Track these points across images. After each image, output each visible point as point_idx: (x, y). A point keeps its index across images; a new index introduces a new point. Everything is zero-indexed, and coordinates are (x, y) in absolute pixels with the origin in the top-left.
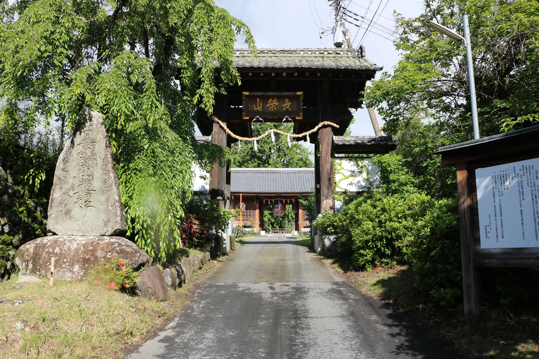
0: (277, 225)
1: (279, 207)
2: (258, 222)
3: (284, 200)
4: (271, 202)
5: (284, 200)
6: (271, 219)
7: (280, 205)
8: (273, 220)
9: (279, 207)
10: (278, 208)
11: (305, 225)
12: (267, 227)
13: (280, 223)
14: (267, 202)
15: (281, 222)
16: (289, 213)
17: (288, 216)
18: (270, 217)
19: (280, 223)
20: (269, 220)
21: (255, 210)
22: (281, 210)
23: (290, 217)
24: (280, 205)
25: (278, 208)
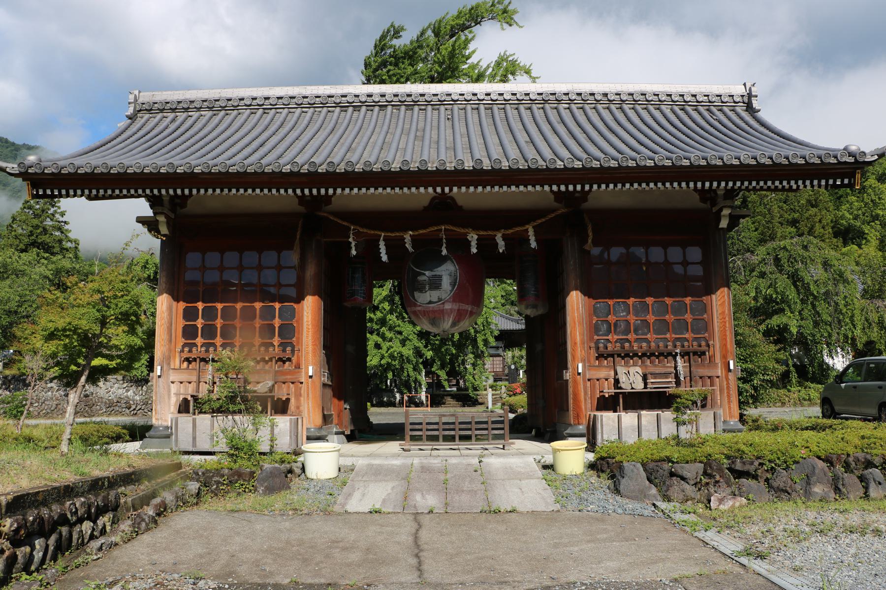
0: (442, 367)
1: (446, 282)
2: (311, 364)
3: (473, 237)
4: (395, 247)
5: (473, 237)
6: (424, 351)
7: (447, 272)
8: (429, 354)
9: (446, 282)
10: (435, 284)
11: (609, 390)
12: (412, 373)
13: (452, 362)
14: (370, 248)
15: (454, 358)
16: (476, 332)
17: (474, 341)
18: (420, 345)
19: (452, 362)
20: (418, 353)
21: (299, 299)
22: (458, 297)
23: (481, 344)
24: (447, 272)
25: (435, 284)
